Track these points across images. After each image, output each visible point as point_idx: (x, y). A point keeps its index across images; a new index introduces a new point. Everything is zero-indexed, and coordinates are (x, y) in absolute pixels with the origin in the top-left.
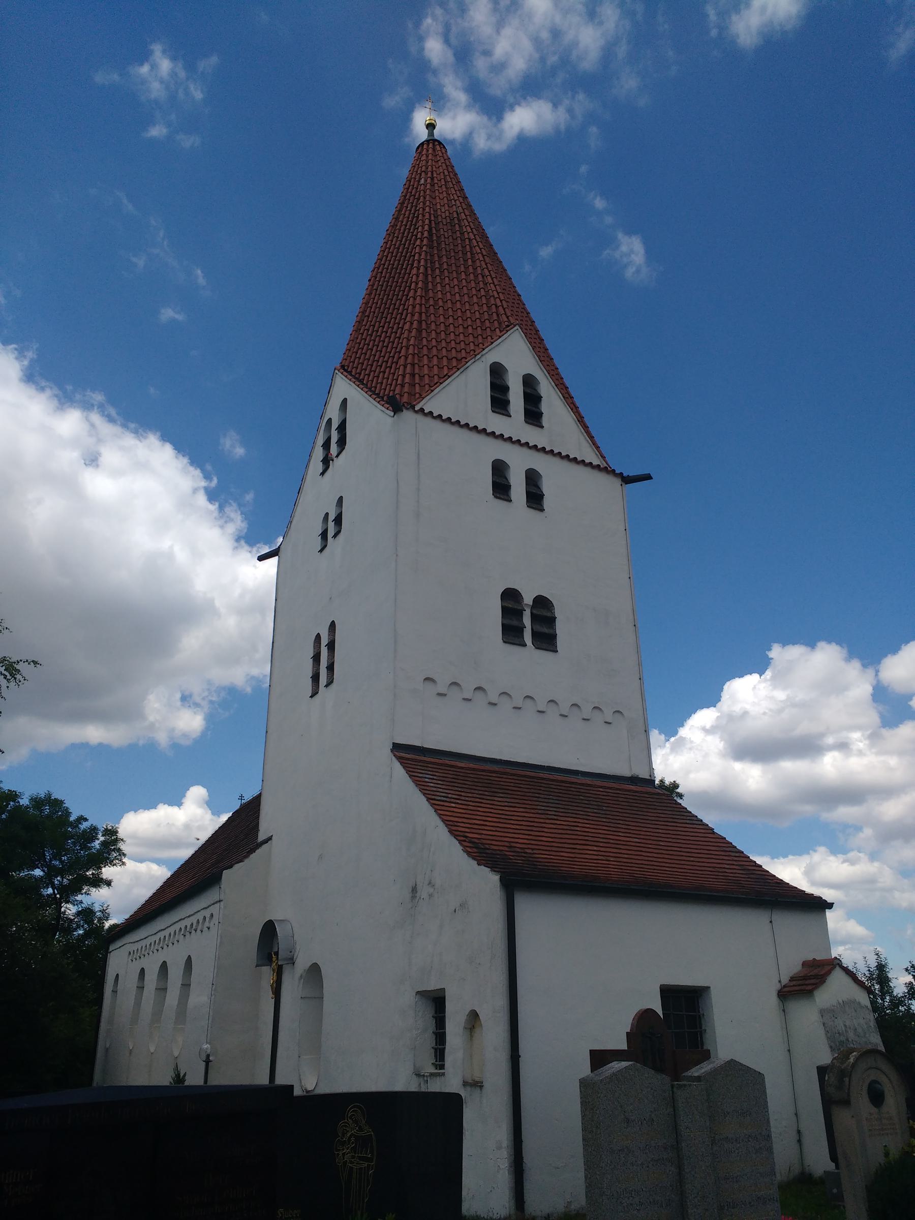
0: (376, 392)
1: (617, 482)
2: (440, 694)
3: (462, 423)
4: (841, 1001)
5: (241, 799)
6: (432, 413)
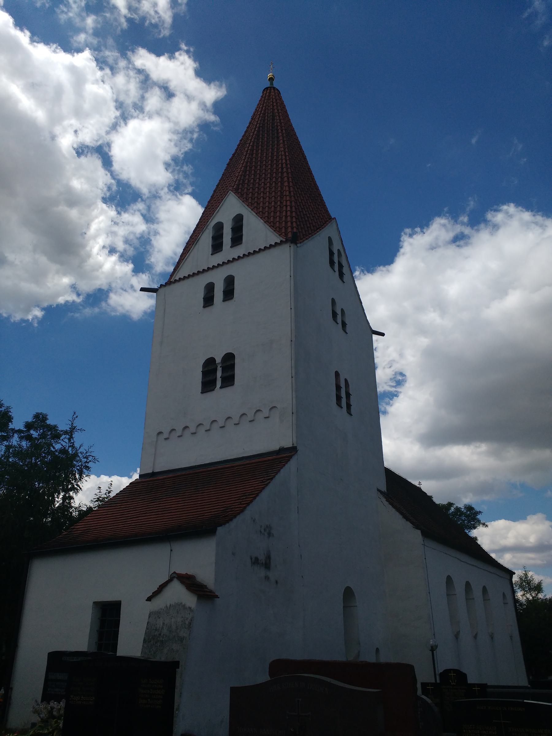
2: (166, 439)
3: (242, 256)
4: (168, 605)
5: (420, 484)
6: (223, 262)
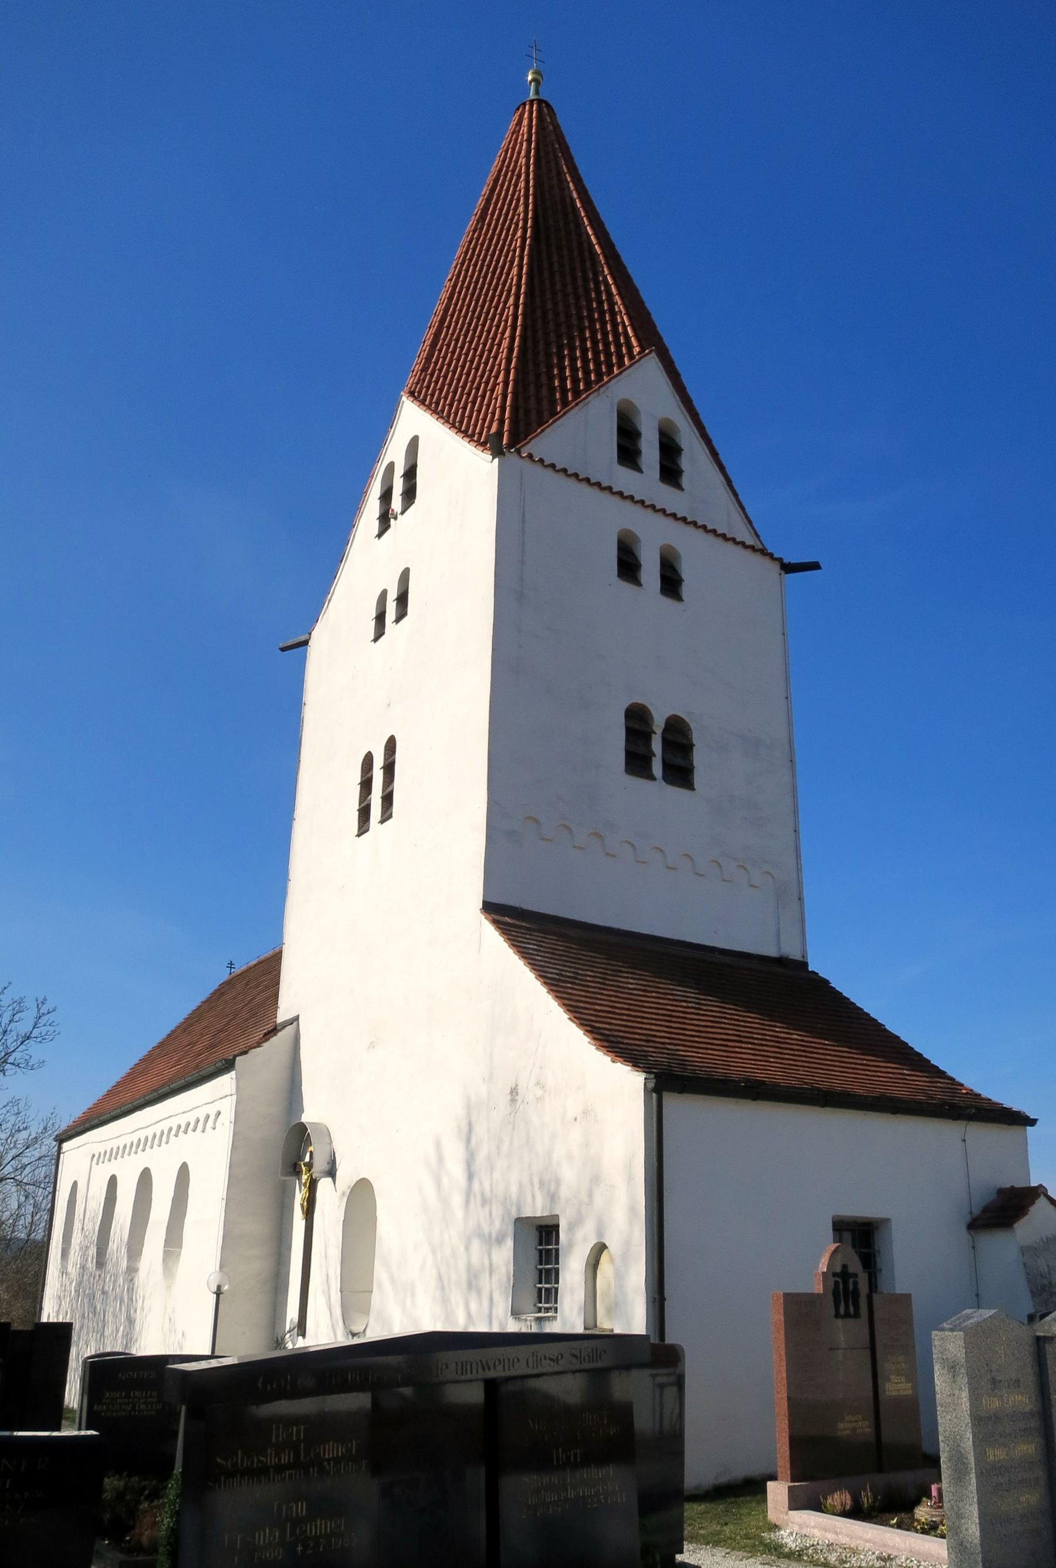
0: (463, 429)
1: (776, 567)
5: (231, 967)
